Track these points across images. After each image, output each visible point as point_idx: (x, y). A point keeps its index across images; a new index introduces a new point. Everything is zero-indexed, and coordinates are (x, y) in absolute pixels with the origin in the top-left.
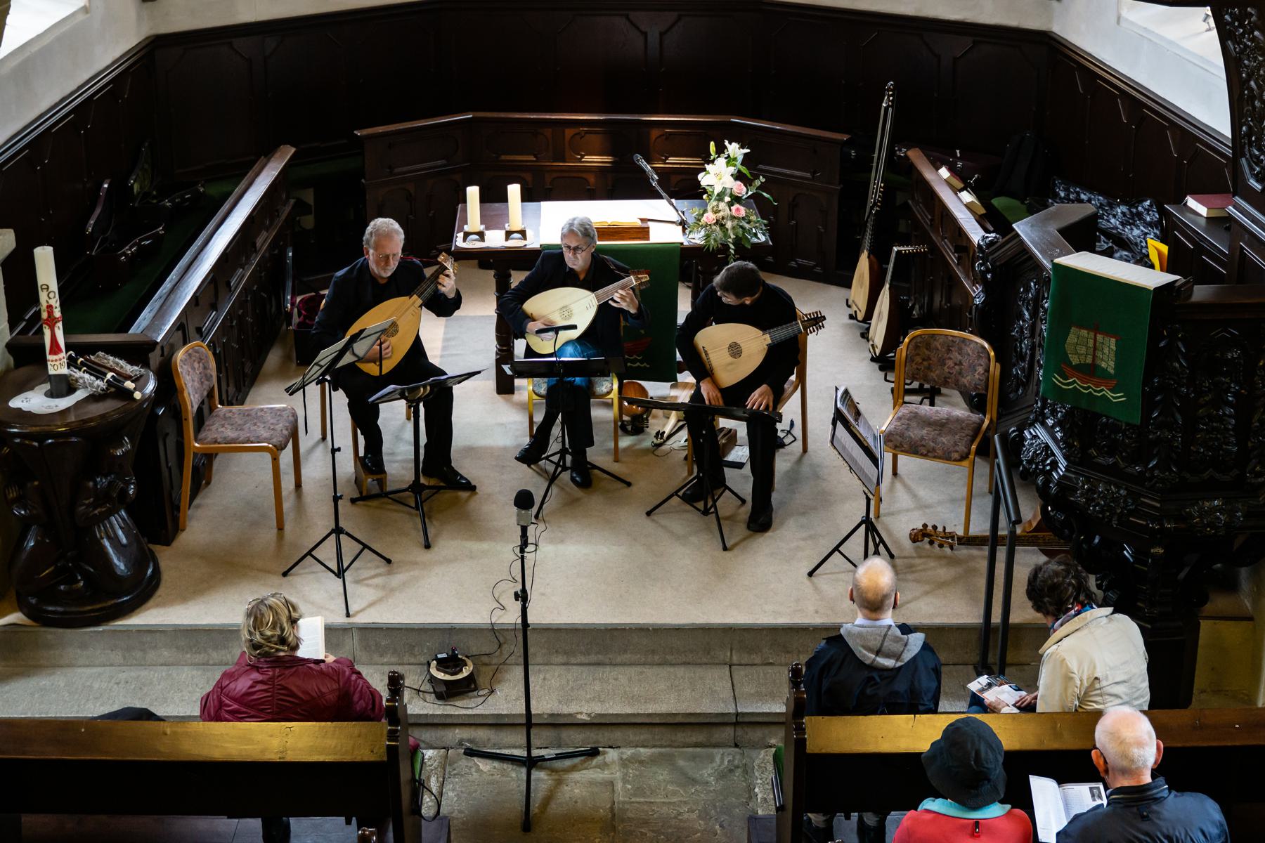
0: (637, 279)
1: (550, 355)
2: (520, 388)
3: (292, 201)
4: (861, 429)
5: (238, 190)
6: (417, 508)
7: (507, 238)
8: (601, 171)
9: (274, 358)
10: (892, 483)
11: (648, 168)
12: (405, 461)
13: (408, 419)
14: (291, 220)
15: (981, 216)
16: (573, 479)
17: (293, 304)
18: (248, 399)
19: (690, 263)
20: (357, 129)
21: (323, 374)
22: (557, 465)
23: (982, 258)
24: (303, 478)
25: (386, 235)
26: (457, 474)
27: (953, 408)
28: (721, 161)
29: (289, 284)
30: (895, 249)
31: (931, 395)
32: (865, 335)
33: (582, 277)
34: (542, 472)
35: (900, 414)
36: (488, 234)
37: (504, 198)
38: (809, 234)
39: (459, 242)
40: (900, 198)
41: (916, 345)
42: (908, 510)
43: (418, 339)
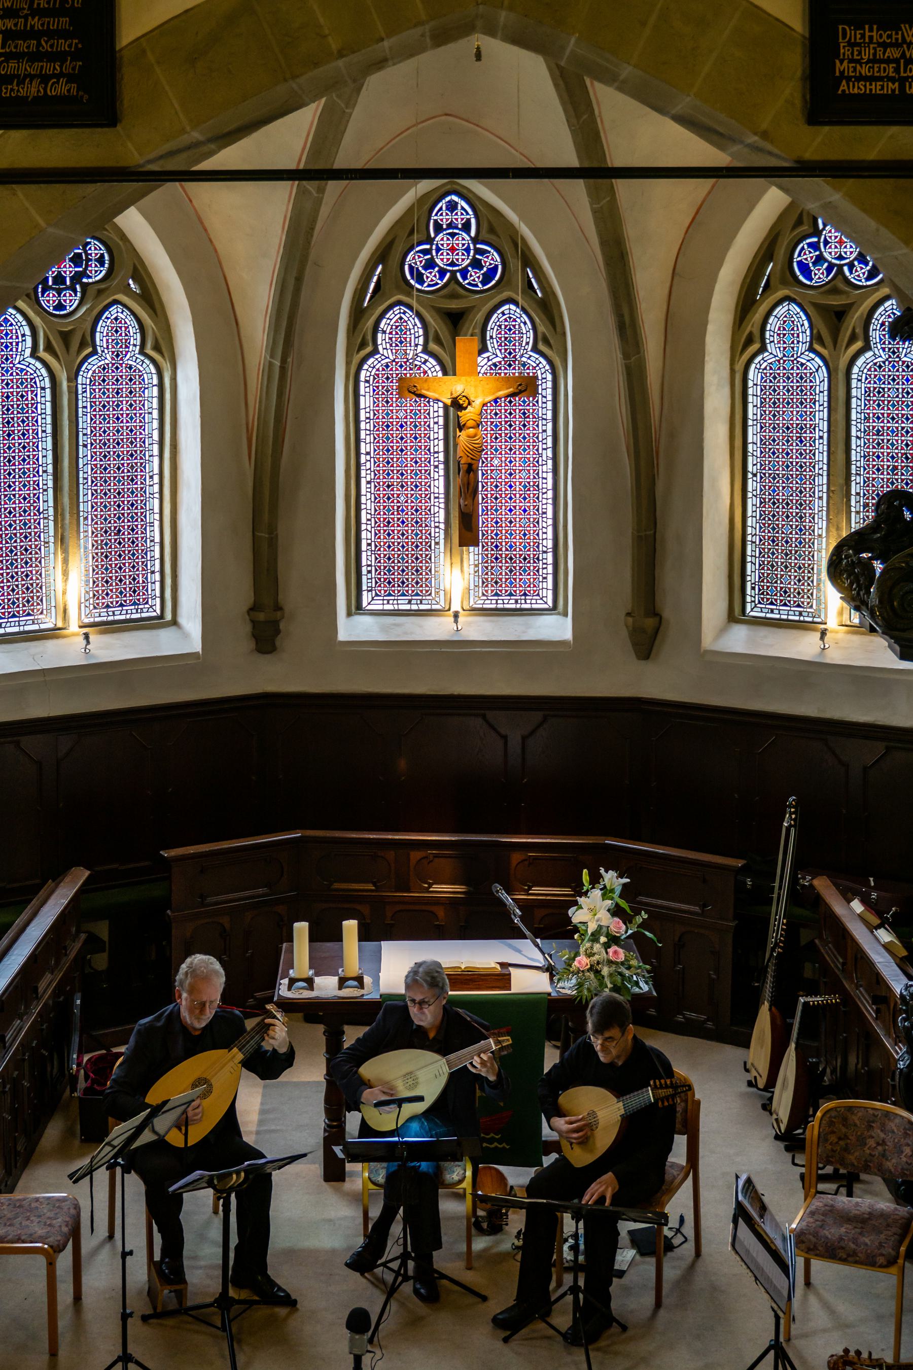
0: (497, 1042)
1: (391, 1133)
2: (353, 1174)
3: (83, 936)
4: (768, 1228)
5: (19, 922)
6: (223, 1329)
7: (340, 988)
8: (452, 903)
9: (53, 1132)
10: (805, 1296)
11: (508, 900)
12: (212, 1267)
13: (216, 1212)
14: (81, 960)
15: (902, 959)
16: (416, 1292)
17: (79, 1065)
18: (21, 1184)
19: (557, 1016)
20: (164, 849)
21: (115, 1157)
22: (397, 1273)
23: (906, 1012)
24: (84, 1288)
25: (202, 977)
26: (273, 1284)
27: (875, 1199)
28: (597, 893)
29: (76, 1039)
30: (802, 1000)
31: (848, 1182)
32: (767, 1107)
33: (432, 1035)
34: (378, 1283)
35: (813, 1207)
36: (318, 980)
37: (337, 936)
38: (704, 982)
39: (283, 990)
40: (805, 936)
41: (833, 1120)
42: (825, 1331)
43: (231, 1113)
